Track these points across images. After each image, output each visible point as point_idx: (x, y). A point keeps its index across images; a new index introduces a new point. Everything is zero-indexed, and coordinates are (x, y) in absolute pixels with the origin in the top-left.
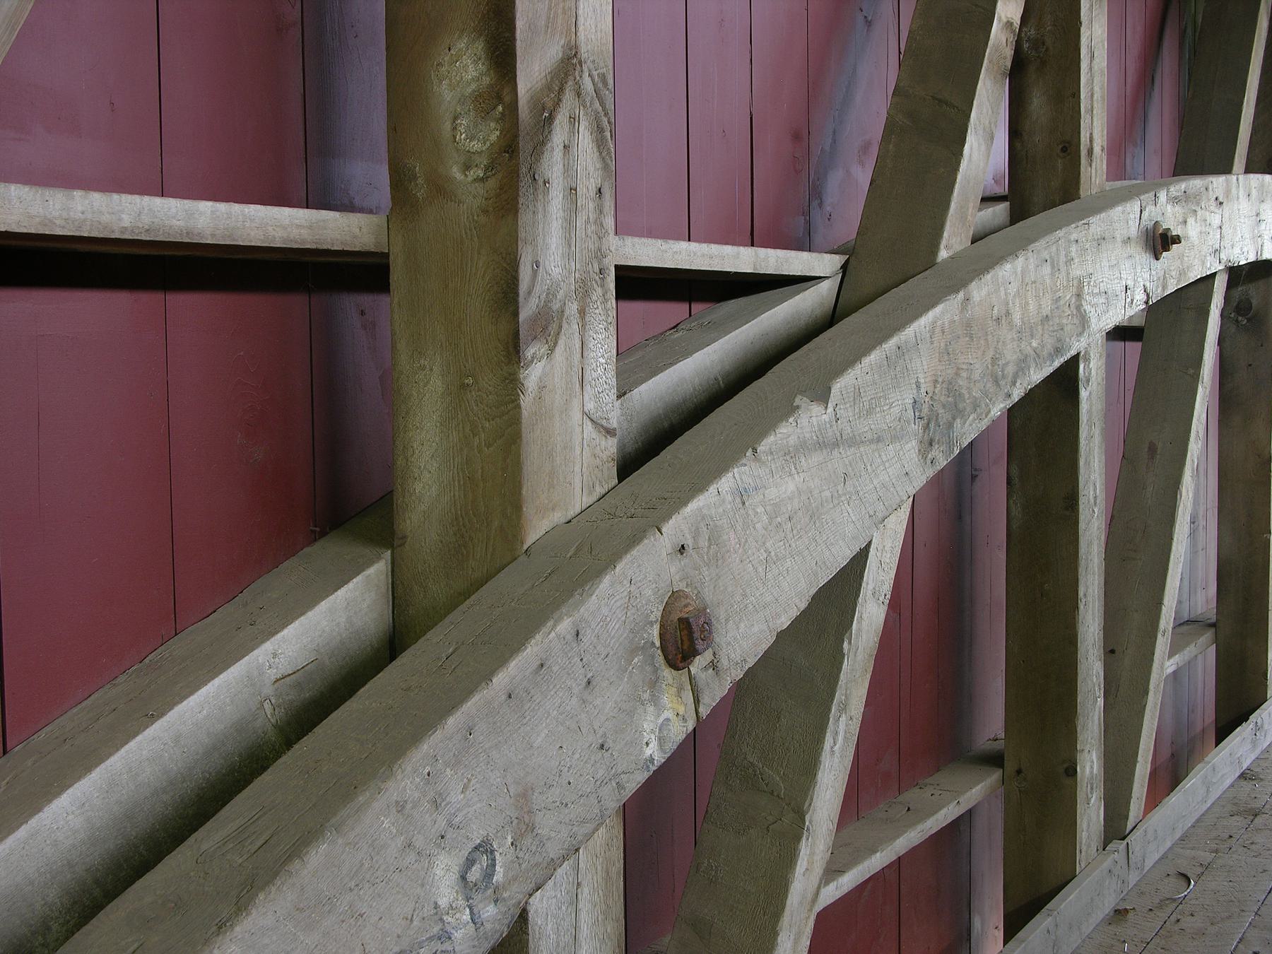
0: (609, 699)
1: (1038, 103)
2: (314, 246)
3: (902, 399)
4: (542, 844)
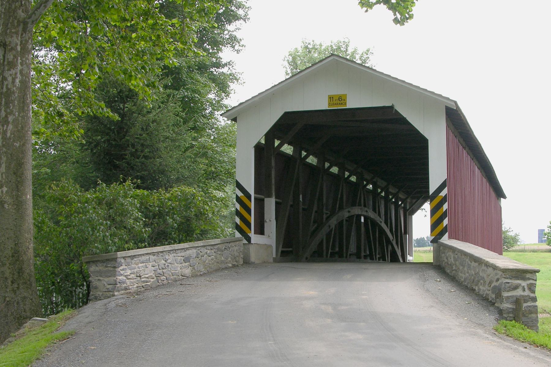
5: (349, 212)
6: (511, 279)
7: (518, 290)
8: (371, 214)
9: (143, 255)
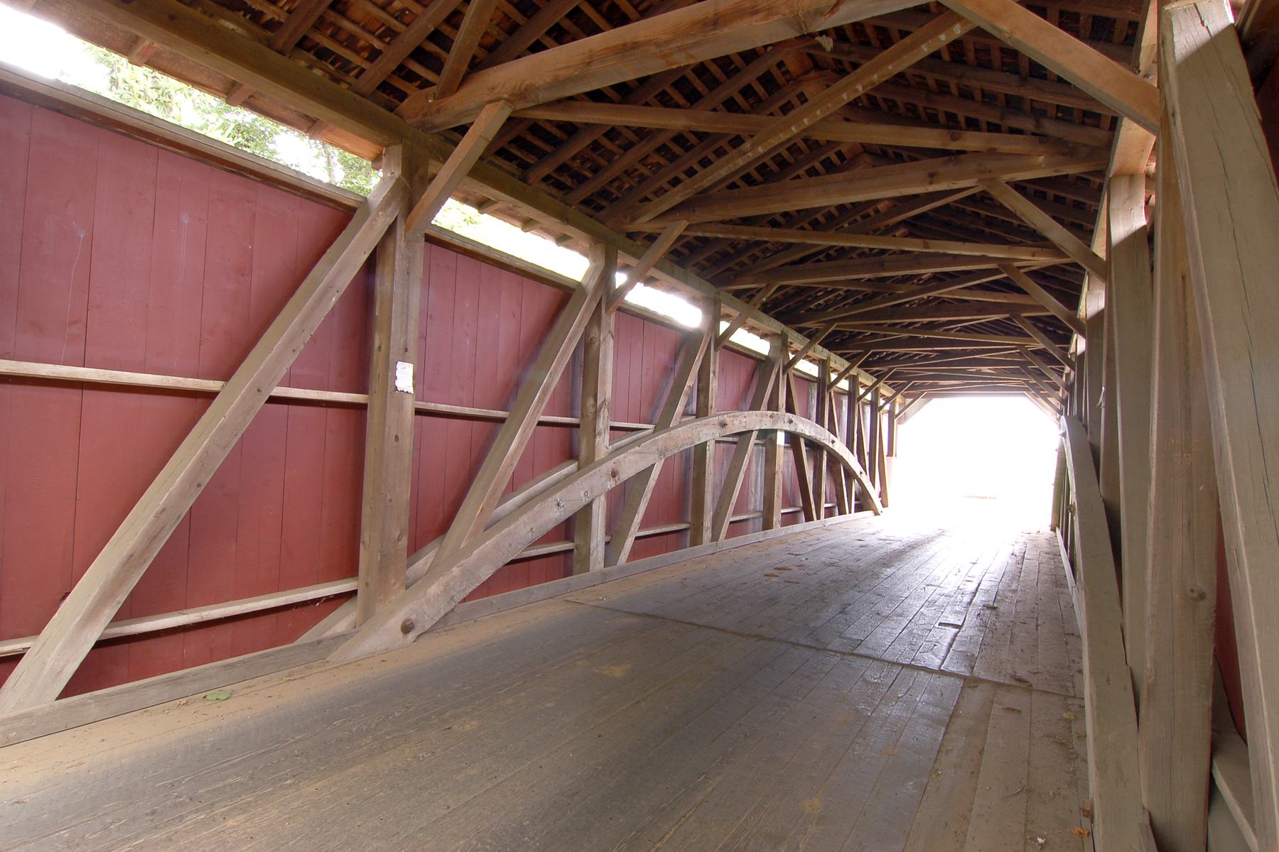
0: (604, 479)
1: (702, 398)
2: (663, 317)
3: (654, 448)
4: (438, 111)
5: (723, 425)
8: (808, 428)
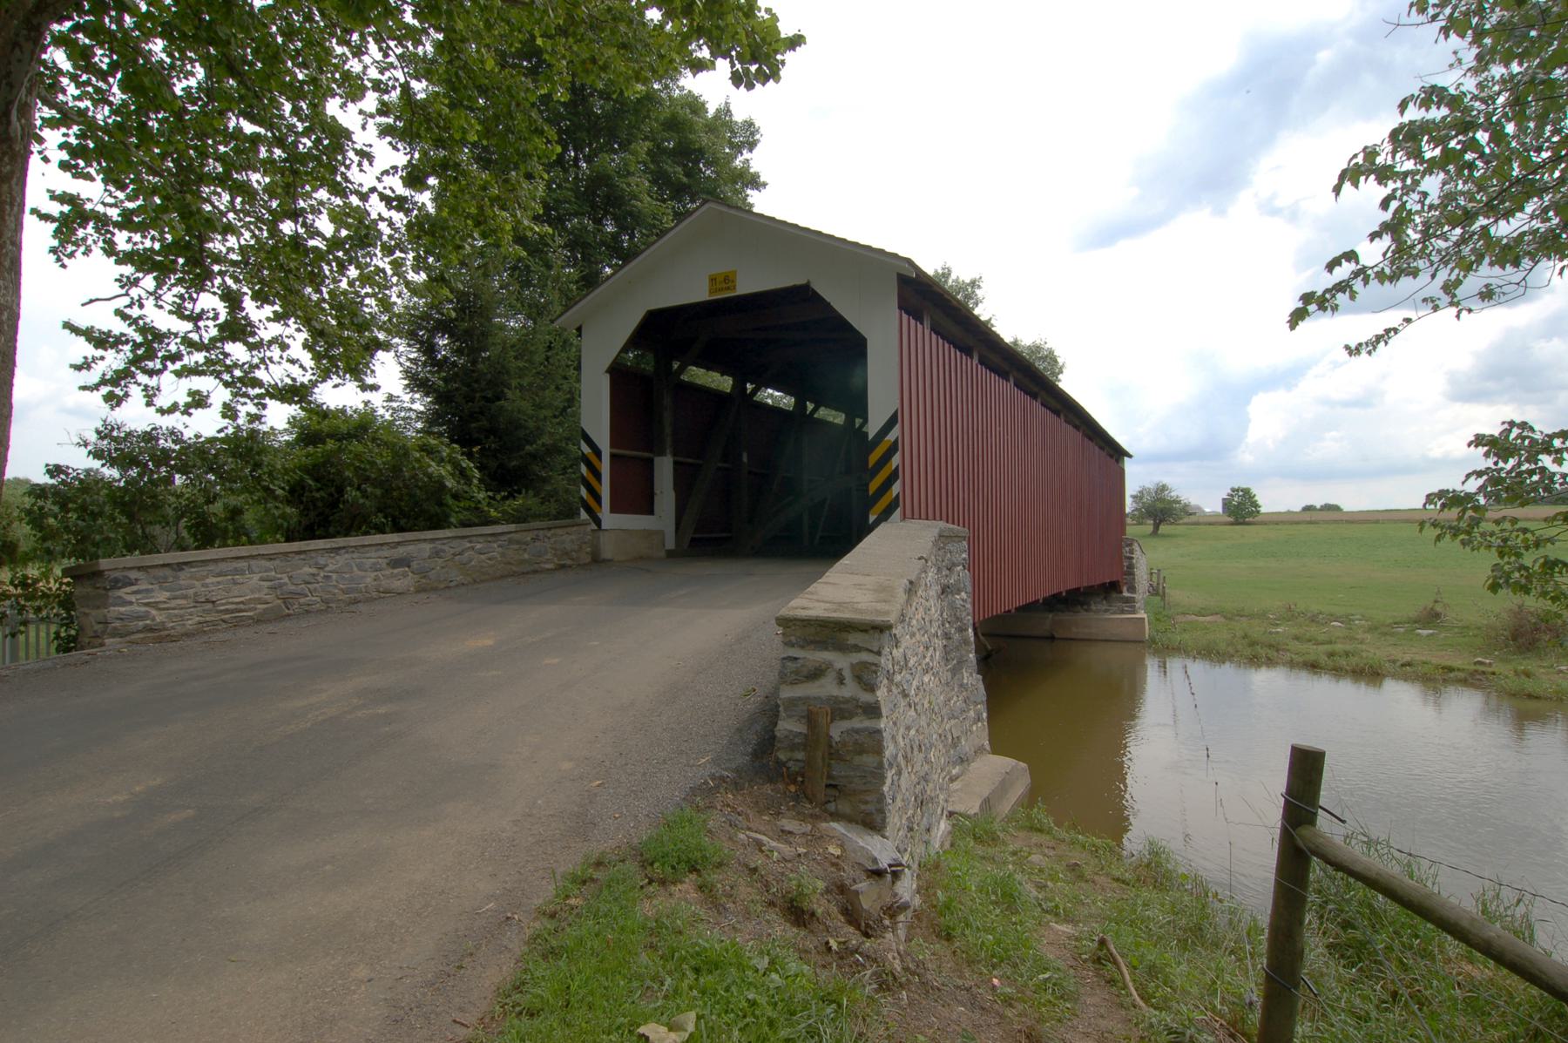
6: (802, 647)
7: (823, 681)
9: (223, 560)
